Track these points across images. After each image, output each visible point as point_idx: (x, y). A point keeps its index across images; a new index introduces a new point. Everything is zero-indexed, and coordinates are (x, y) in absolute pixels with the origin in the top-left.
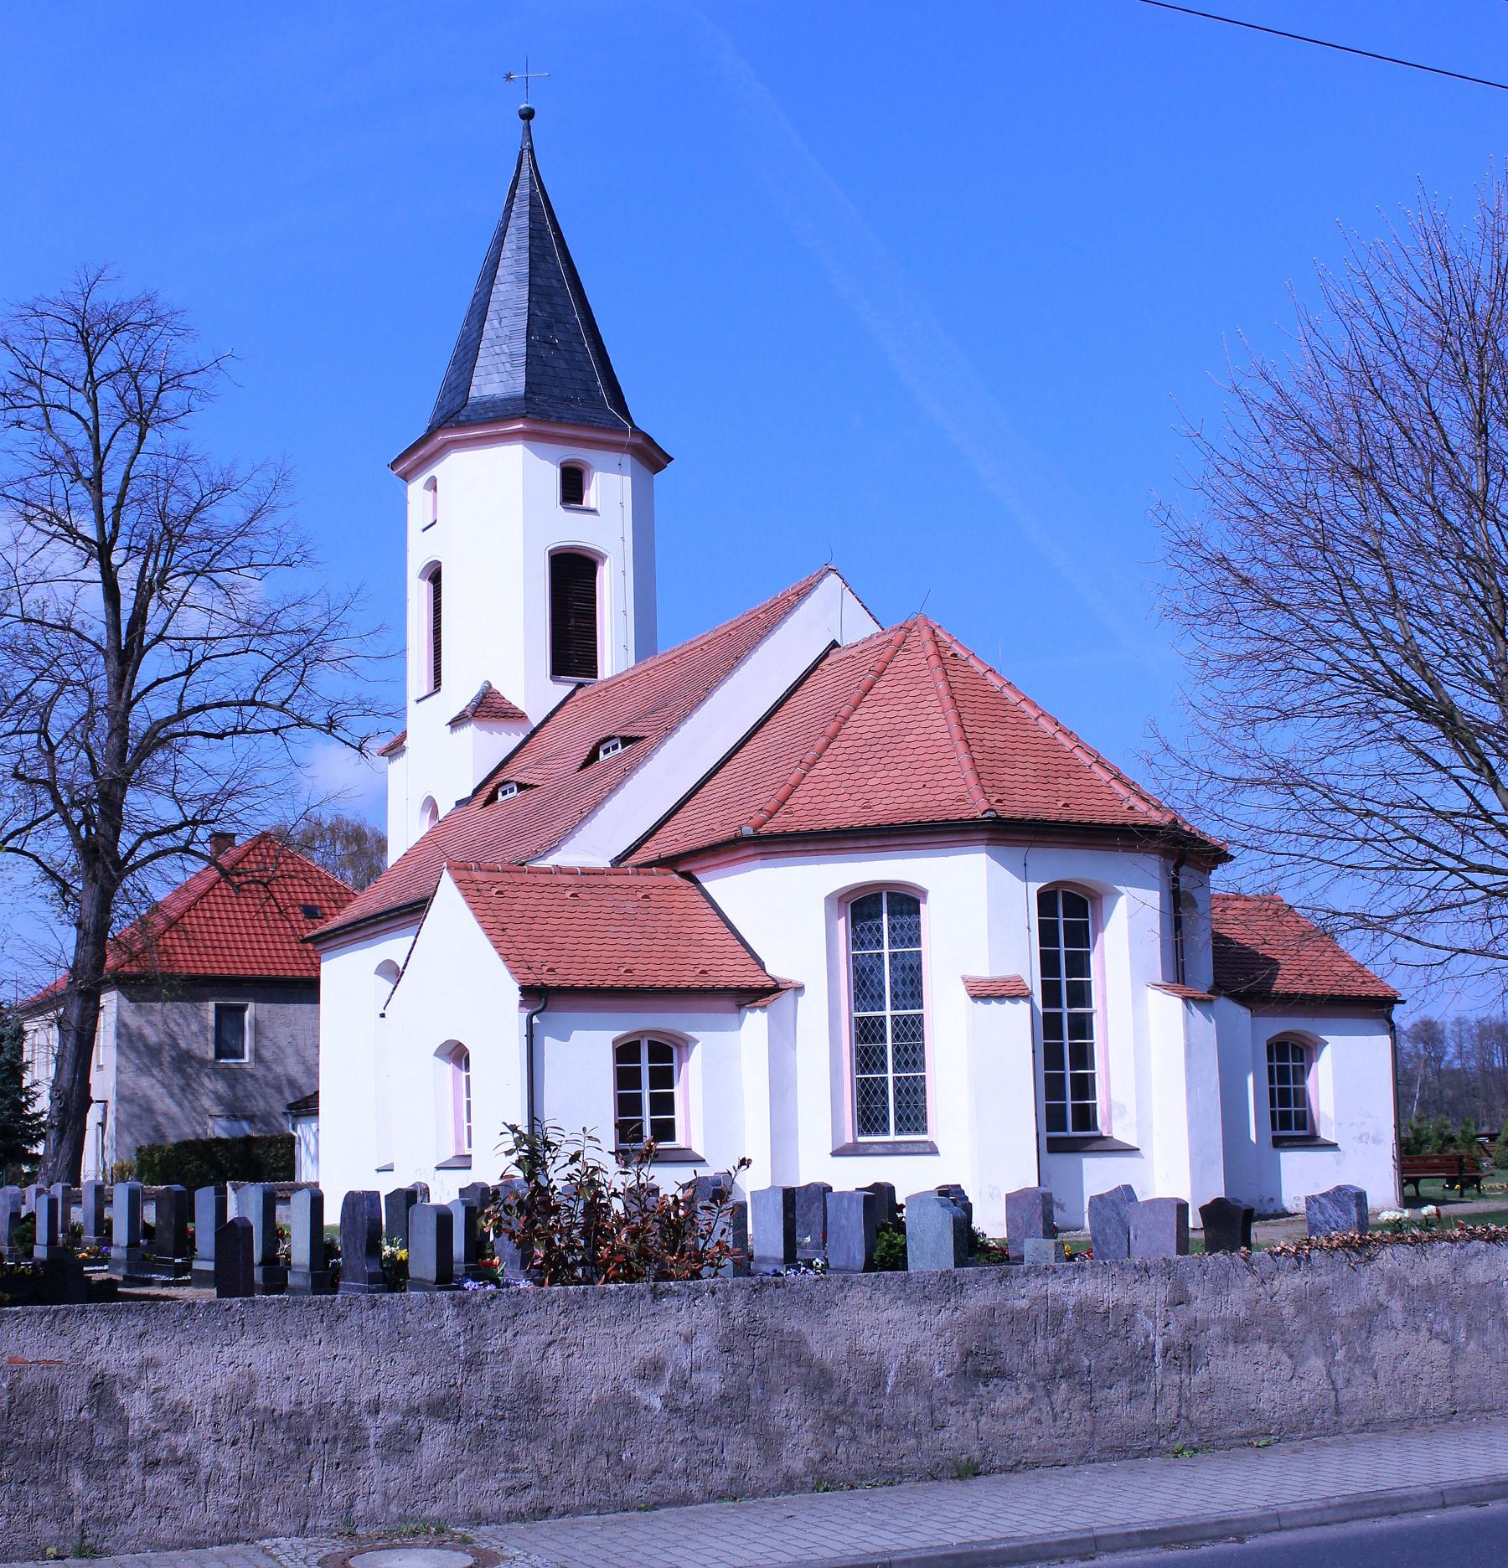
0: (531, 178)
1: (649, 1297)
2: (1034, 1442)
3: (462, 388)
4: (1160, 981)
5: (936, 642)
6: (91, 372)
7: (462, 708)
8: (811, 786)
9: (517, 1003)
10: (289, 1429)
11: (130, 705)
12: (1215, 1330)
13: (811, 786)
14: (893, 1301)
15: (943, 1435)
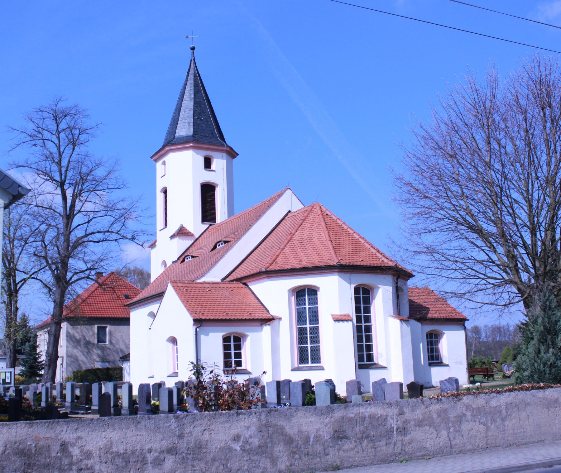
0: (194, 68)
1: (235, 415)
2: (357, 459)
3: (173, 133)
4: (393, 315)
5: (321, 210)
6: (58, 129)
10: (123, 458)
11: (70, 232)
12: (412, 423)
13: (282, 256)
15: (328, 457)
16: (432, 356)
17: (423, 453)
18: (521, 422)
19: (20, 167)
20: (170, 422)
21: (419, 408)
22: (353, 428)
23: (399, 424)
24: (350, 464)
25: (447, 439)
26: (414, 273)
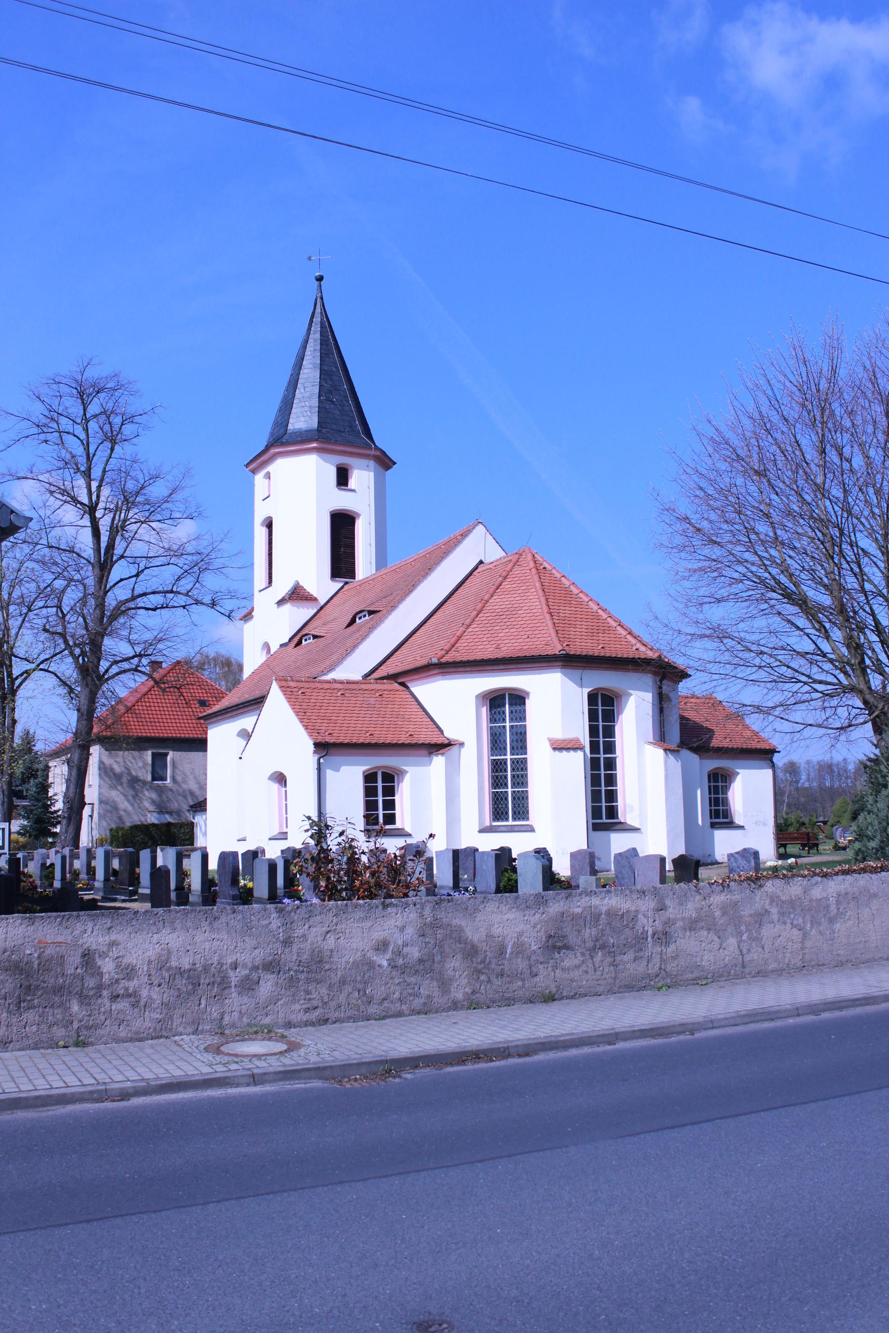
0: (321, 313)
1: (381, 907)
2: (584, 983)
3: (283, 425)
4: (652, 741)
6: (85, 414)
7: (283, 595)
8: (468, 637)
10: (188, 978)
11: (106, 593)
12: (680, 924)
13: (468, 637)
15: (537, 979)
18: (861, 925)
19: (19, 479)
20: (270, 918)
22: (579, 931)
23: (657, 925)
25: (737, 952)
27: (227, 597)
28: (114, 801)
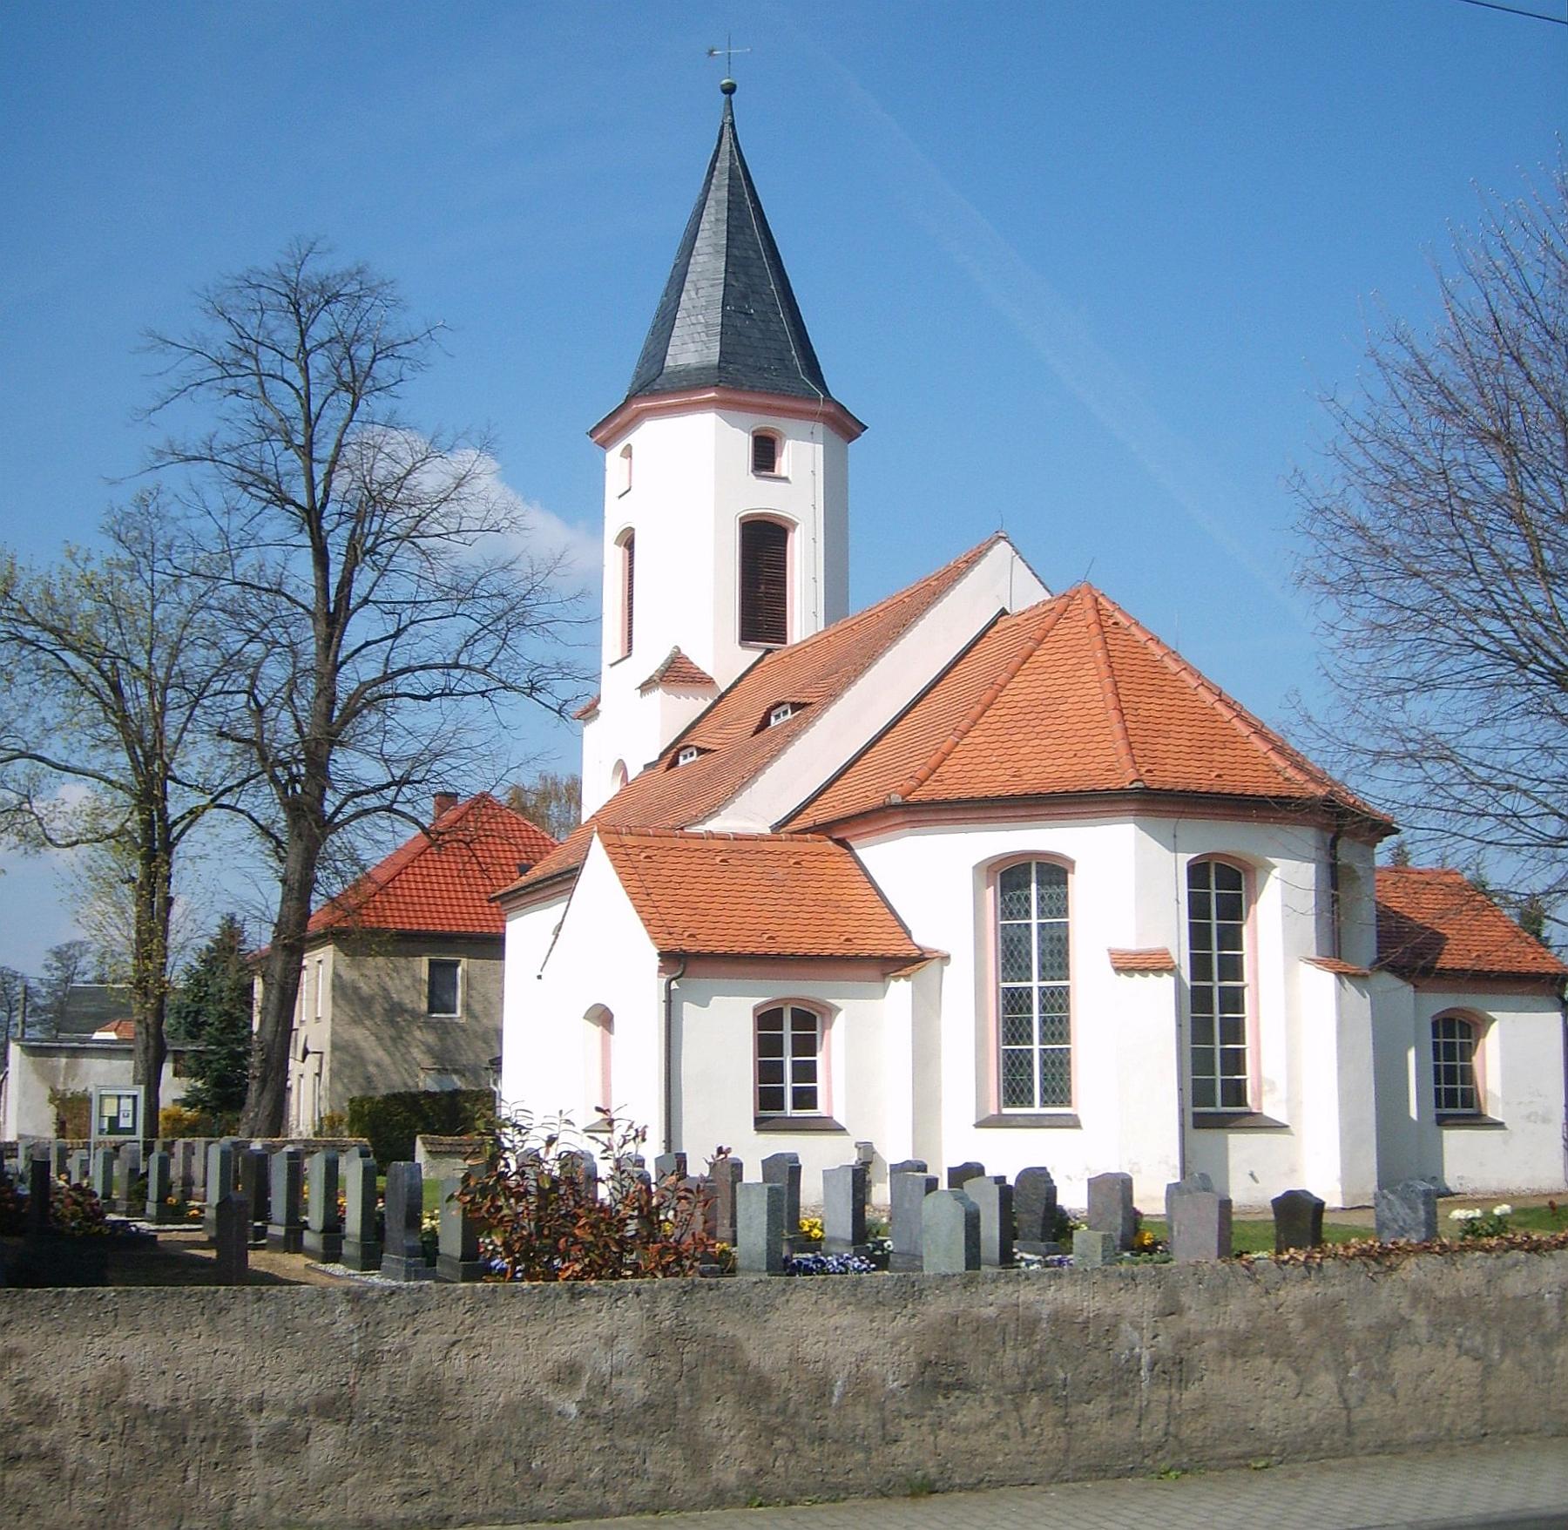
0: (731, 151)
1: (566, 1297)
2: (1000, 1459)
3: (658, 358)
4: (1314, 956)
5: (1098, 611)
6: (303, 343)
7: (652, 672)
9: (656, 969)
10: (162, 1427)
11: (337, 668)
12: (1211, 1343)
14: (842, 1306)
16: (1451, 1094)
17: (1244, 1447)
19: (188, 459)
21: (1239, 1293)
22: (991, 1354)
23: (1161, 1345)
24: (975, 1475)
25: (1336, 1403)
26: (1399, 819)
27: (555, 676)
28: (357, 1048)
